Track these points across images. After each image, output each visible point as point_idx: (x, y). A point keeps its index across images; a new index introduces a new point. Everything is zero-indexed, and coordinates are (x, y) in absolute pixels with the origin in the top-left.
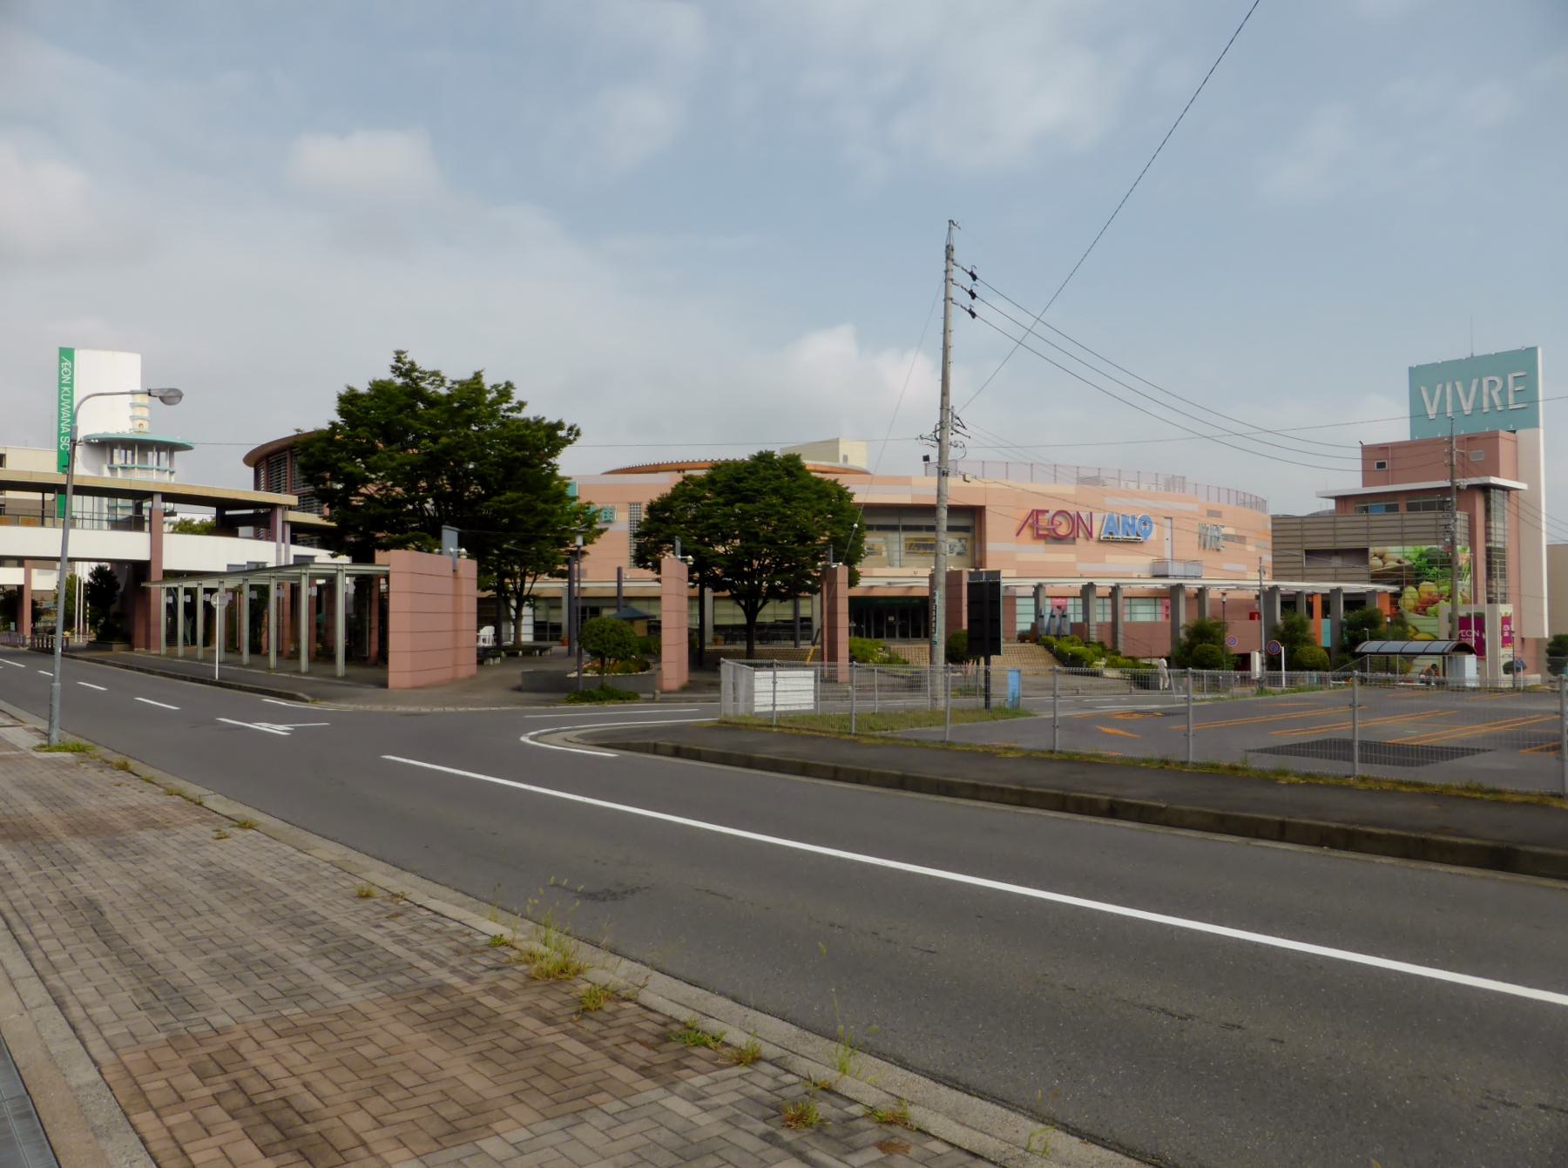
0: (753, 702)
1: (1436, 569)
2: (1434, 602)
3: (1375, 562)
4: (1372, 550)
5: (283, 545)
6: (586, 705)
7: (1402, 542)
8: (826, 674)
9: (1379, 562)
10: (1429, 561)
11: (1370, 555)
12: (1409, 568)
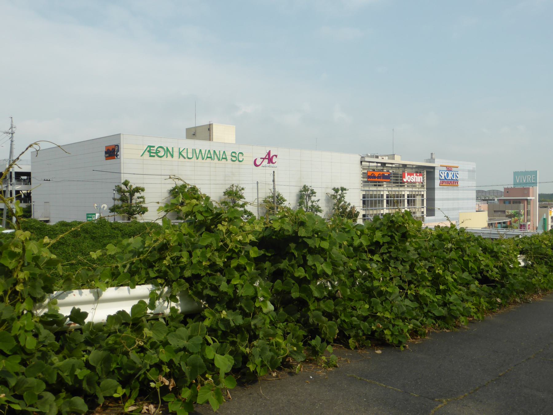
3: (507, 213)
4: (506, 211)
12: (513, 214)
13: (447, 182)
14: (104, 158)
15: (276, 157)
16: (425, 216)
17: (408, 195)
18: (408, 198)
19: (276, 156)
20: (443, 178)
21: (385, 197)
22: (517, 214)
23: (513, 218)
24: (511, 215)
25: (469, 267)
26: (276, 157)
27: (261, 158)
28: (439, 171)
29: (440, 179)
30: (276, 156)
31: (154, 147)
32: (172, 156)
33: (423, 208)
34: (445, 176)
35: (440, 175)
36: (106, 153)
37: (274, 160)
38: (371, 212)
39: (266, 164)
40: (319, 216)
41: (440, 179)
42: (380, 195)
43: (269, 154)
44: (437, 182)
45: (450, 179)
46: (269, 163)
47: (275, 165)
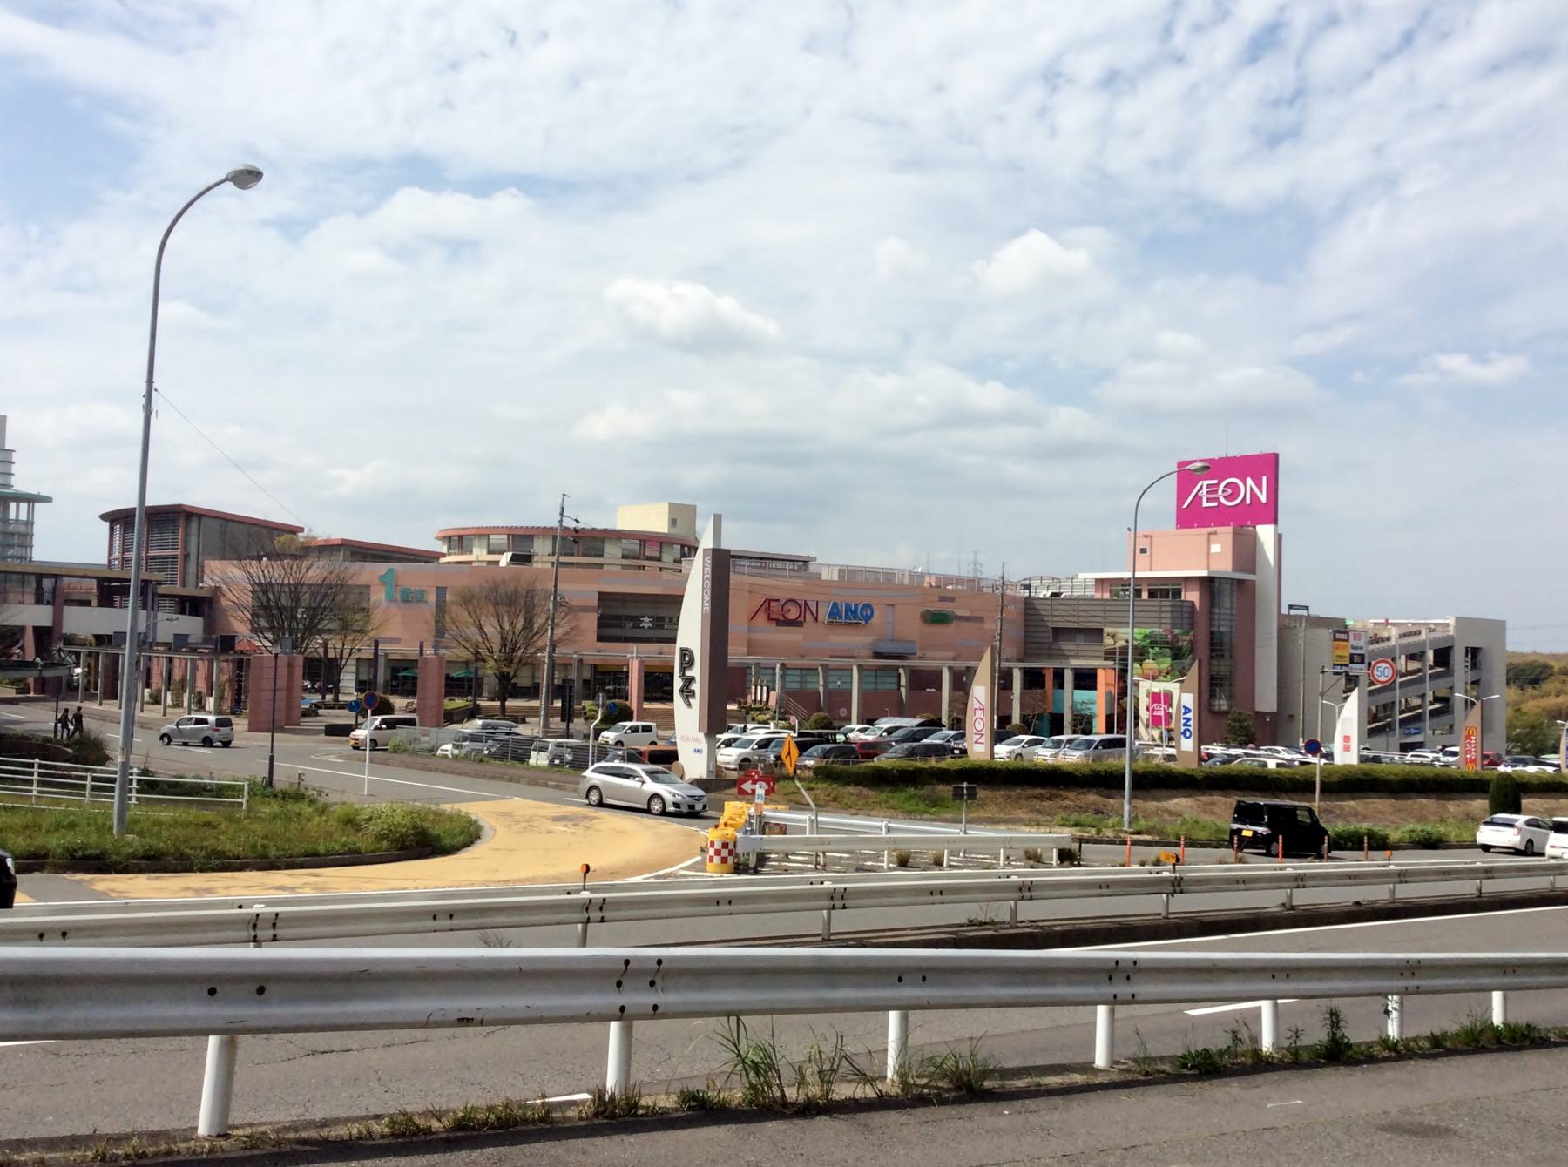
0: (319, 660)
3: (1108, 641)
4: (1107, 630)
5: (144, 613)
8: (1442, 1108)
9: (1112, 641)
10: (1151, 643)
11: (1105, 635)
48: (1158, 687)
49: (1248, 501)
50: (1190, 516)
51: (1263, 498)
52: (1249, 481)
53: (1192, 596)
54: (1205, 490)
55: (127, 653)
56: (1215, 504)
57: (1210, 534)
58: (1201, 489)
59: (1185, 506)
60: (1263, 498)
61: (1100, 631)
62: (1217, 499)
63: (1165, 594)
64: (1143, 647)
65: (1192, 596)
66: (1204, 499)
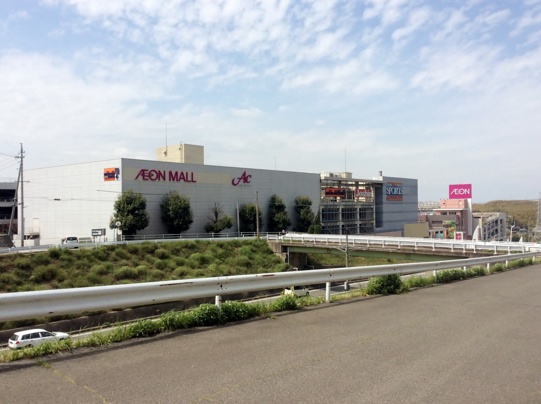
1: (454, 225)
2: (453, 230)
3: (443, 223)
4: (443, 221)
6: (490, 249)
7: (448, 220)
12: (449, 224)
13: (392, 196)
14: (103, 179)
15: (251, 177)
16: (375, 227)
17: (342, 209)
18: (359, 211)
19: (250, 176)
20: (390, 193)
21: (340, 211)
22: (453, 224)
23: (449, 228)
24: (448, 225)
25: (537, 252)
26: (251, 177)
27: (238, 178)
28: (386, 187)
29: (387, 194)
30: (250, 176)
31: (148, 170)
32: (164, 179)
33: (373, 220)
34: (391, 192)
35: (387, 191)
36: (105, 175)
37: (249, 179)
38: (329, 224)
39: (242, 183)
40: (422, 215)
41: (387, 194)
42: (336, 209)
43: (244, 174)
44: (385, 197)
45: (396, 194)
46: (244, 182)
47: (249, 184)
48: (458, 233)
49: (465, 194)
50: (452, 196)
51: (469, 193)
52: (466, 190)
53: (459, 214)
54: (456, 191)
55: (228, 238)
56: (458, 194)
57: (459, 201)
58: (455, 191)
59: (451, 194)
60: (469, 193)
61: (442, 222)
62: (458, 193)
63: (452, 213)
64: (451, 224)
65: (459, 214)
66: (456, 193)
